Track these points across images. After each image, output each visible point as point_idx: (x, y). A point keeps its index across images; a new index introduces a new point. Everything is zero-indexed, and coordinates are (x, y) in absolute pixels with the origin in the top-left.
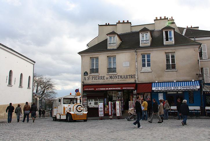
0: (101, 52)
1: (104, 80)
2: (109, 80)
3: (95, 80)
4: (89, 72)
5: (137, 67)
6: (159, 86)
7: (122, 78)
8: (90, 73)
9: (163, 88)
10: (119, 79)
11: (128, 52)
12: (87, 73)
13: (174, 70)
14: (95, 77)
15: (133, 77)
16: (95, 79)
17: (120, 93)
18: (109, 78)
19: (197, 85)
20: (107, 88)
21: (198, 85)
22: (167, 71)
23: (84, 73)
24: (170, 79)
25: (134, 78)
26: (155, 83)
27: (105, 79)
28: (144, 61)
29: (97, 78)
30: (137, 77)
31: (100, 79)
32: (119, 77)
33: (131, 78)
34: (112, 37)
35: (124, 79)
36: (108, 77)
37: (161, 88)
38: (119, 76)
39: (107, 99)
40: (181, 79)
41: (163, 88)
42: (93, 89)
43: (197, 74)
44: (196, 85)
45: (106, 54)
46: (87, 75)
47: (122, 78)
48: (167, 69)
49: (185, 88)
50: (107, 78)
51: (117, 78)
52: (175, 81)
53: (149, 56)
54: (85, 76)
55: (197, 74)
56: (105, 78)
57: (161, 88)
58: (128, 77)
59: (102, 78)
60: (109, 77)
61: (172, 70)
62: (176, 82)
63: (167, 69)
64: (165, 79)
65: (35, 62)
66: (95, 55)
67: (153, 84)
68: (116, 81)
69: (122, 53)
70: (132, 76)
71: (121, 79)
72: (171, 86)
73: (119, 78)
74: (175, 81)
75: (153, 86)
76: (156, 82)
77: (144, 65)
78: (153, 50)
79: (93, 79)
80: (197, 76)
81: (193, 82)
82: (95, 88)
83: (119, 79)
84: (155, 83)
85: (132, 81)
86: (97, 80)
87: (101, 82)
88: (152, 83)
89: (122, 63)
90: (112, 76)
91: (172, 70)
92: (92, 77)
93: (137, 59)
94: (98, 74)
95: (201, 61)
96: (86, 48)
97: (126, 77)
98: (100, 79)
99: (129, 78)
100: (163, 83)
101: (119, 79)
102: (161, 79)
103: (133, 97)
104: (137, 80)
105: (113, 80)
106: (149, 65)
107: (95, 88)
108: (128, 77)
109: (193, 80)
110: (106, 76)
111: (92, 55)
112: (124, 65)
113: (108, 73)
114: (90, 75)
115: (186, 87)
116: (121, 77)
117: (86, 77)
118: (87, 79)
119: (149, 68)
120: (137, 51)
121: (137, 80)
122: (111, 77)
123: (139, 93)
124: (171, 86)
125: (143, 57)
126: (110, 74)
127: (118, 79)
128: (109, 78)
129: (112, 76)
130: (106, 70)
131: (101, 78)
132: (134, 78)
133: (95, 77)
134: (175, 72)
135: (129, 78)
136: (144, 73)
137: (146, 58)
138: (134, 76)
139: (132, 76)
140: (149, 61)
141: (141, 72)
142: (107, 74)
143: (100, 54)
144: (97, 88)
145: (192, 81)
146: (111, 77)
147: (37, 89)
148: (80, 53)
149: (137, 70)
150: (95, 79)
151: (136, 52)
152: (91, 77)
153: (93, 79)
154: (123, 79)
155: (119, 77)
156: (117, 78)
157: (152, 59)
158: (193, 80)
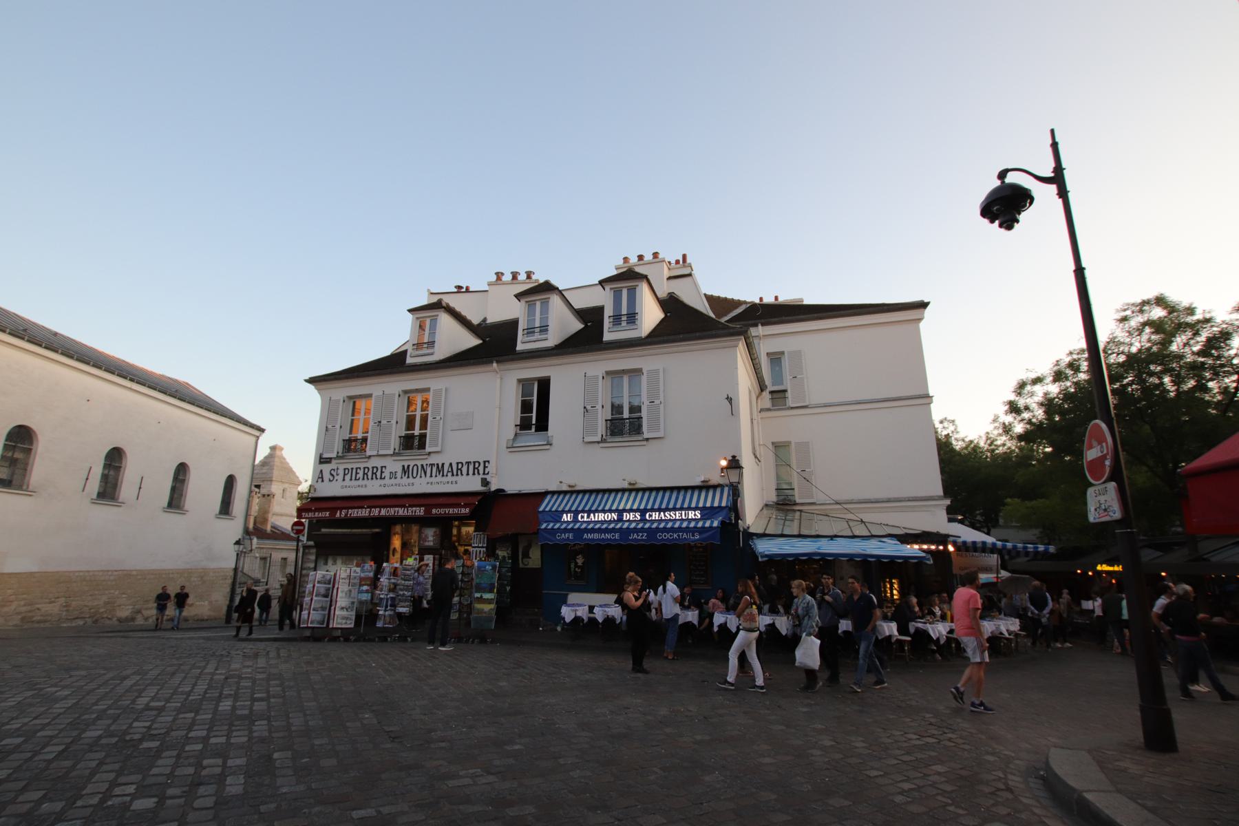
1: (382, 482)
3: (354, 483)
7: (443, 476)
10: (433, 479)
14: (354, 471)
15: (481, 469)
16: (353, 478)
18: (399, 475)
20: (375, 507)
29: (360, 475)
31: (370, 477)
33: (474, 474)
34: (538, 304)
47: (443, 476)
60: (401, 468)
68: (421, 485)
73: (434, 474)
79: (348, 477)
82: (428, 508)
83: (431, 476)
85: (470, 484)
86: (360, 482)
87: (373, 488)
95: (645, 428)
96: (615, 272)
98: (370, 477)
99: (468, 474)
101: (431, 476)
105: (450, 478)
107: (333, 510)
108: (464, 470)
117: (327, 468)
118: (327, 476)
128: (399, 475)
129: (409, 466)
131: (373, 473)
132: (381, 478)
133: (354, 471)
135: (468, 474)
138: (485, 467)
139: (477, 465)
144: (341, 509)
147: (531, 534)
150: (353, 478)
153: (348, 477)
154: (445, 479)
155: (435, 469)
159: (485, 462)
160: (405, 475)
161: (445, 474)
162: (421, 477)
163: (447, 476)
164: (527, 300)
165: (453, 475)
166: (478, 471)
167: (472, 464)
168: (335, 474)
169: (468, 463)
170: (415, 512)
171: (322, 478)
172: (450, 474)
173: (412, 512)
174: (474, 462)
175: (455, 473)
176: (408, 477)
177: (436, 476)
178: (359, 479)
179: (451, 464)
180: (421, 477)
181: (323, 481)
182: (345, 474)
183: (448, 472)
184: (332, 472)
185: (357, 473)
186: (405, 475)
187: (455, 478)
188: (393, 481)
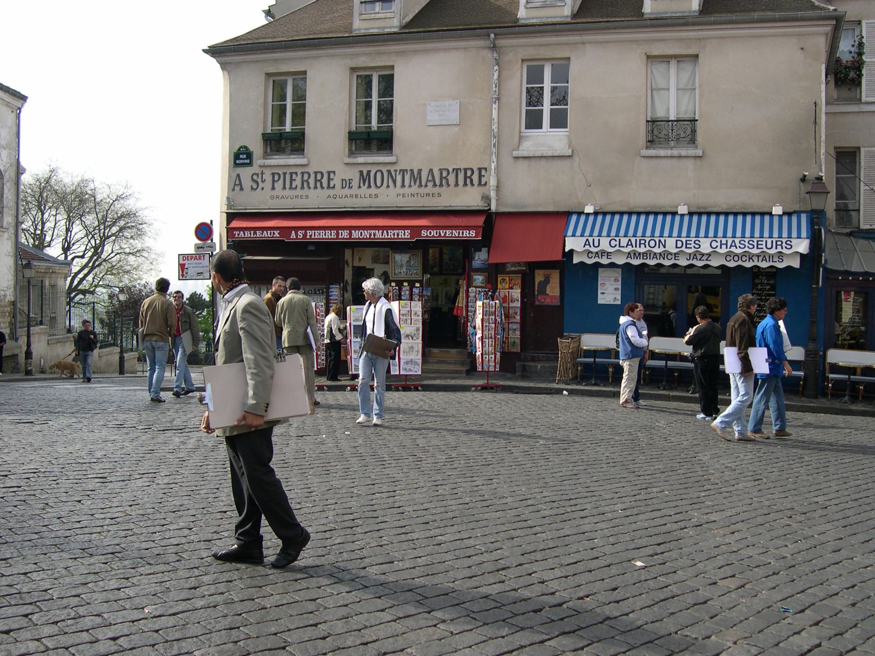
0: (461, 38)
1: (331, 192)
2: (355, 191)
3: (288, 192)
4: (256, 147)
5: (495, 127)
6: (604, 233)
8: (266, 155)
9: (624, 241)
10: (406, 190)
11: (457, 49)
12: (249, 155)
13: (684, 152)
14: (288, 177)
15: (475, 178)
16: (288, 186)
17: (401, 258)
18: (355, 183)
19: (799, 237)
21: (804, 234)
22: (652, 152)
23: (237, 156)
24: (661, 199)
25: (329, 187)
26: (678, 218)
27: (338, 185)
28: (534, 97)
29: (298, 182)
30: (493, 182)
31: (312, 185)
32: (407, 177)
33: (465, 184)
35: (430, 189)
36: (353, 174)
37: (714, 244)
38: (403, 172)
39: (344, 289)
40: (721, 200)
41: (624, 241)
42: (407, 232)
43: (804, 179)
44: (794, 234)
45: (346, 56)
46: (250, 164)
47: (420, 186)
48: (651, 142)
49: (734, 245)
50: (347, 184)
51: (415, 183)
52: (683, 210)
53: (561, 73)
54: (240, 170)
55: (804, 179)
56: (337, 181)
57: (714, 244)
58: (452, 178)
59: (323, 180)
60: (358, 175)
61: (675, 152)
62: (691, 214)
63: (651, 142)
64: (640, 198)
65: (24, 98)
66: (290, 62)
67: (574, 218)
69: (425, 51)
70: (319, 177)
71: (415, 189)
72: (666, 233)
73: (407, 182)
74: (683, 210)
75: (570, 233)
76: (589, 209)
77: (534, 121)
78: (584, 43)
79: (279, 185)
80: (805, 188)
81: (776, 220)
83: (403, 186)
84: (678, 218)
86: (298, 192)
88: (568, 214)
89: (425, 105)
90: (369, 172)
91: (675, 152)
92: (273, 174)
93: (499, 85)
94: (391, 159)
97: (441, 178)
98: (312, 185)
99: (457, 184)
100: (749, 218)
101: (403, 186)
102: (617, 200)
103: (469, 285)
104: (493, 194)
105: (373, 191)
106: (559, 120)
108: (452, 178)
109: (777, 210)
110: (343, 173)
111: (276, 60)
112: (433, 118)
113: (351, 153)
114: (261, 162)
115: (737, 241)
116: (416, 177)
117: (246, 173)
118: (247, 183)
119: (560, 132)
120: (501, 42)
121: (493, 194)
122: (365, 178)
123: (504, 265)
124: (666, 233)
125: (535, 75)
126: (361, 160)
127: (399, 190)
128: (355, 183)
129: (369, 172)
130: (341, 142)
131: (316, 181)
132: (329, 187)
133: (288, 177)
134: (690, 163)
135: (457, 184)
136: (533, 163)
137: (547, 85)
138: (480, 176)
139: (469, 173)
140: (560, 98)
141: (515, 154)
142: (347, 160)
143: (316, 57)
145: (770, 214)
146: (365, 178)
148: (214, 51)
149: (498, 146)
150: (288, 186)
151: (494, 48)
152: (268, 176)
154: (423, 190)
155: (407, 177)
156: (394, 182)
157: (576, 88)
158: (777, 210)
159: (480, 170)
160: (415, 183)
161: (423, 183)
162: (388, 186)
163: (426, 186)
164: (272, 70)
165: (435, 185)
166: (308, 183)
167: (463, 172)
168: (259, 180)
169: (457, 171)
170: (398, 235)
171: (240, 184)
172: (430, 184)
173: (394, 235)
174: (466, 170)
175: (438, 182)
176: (369, 186)
177: (410, 186)
178: (296, 188)
179: (431, 171)
180: (388, 186)
181: (242, 189)
182: (274, 181)
183: (428, 181)
184: (255, 177)
185: (292, 180)
186: (415, 183)
187: (437, 190)
188: (347, 191)
